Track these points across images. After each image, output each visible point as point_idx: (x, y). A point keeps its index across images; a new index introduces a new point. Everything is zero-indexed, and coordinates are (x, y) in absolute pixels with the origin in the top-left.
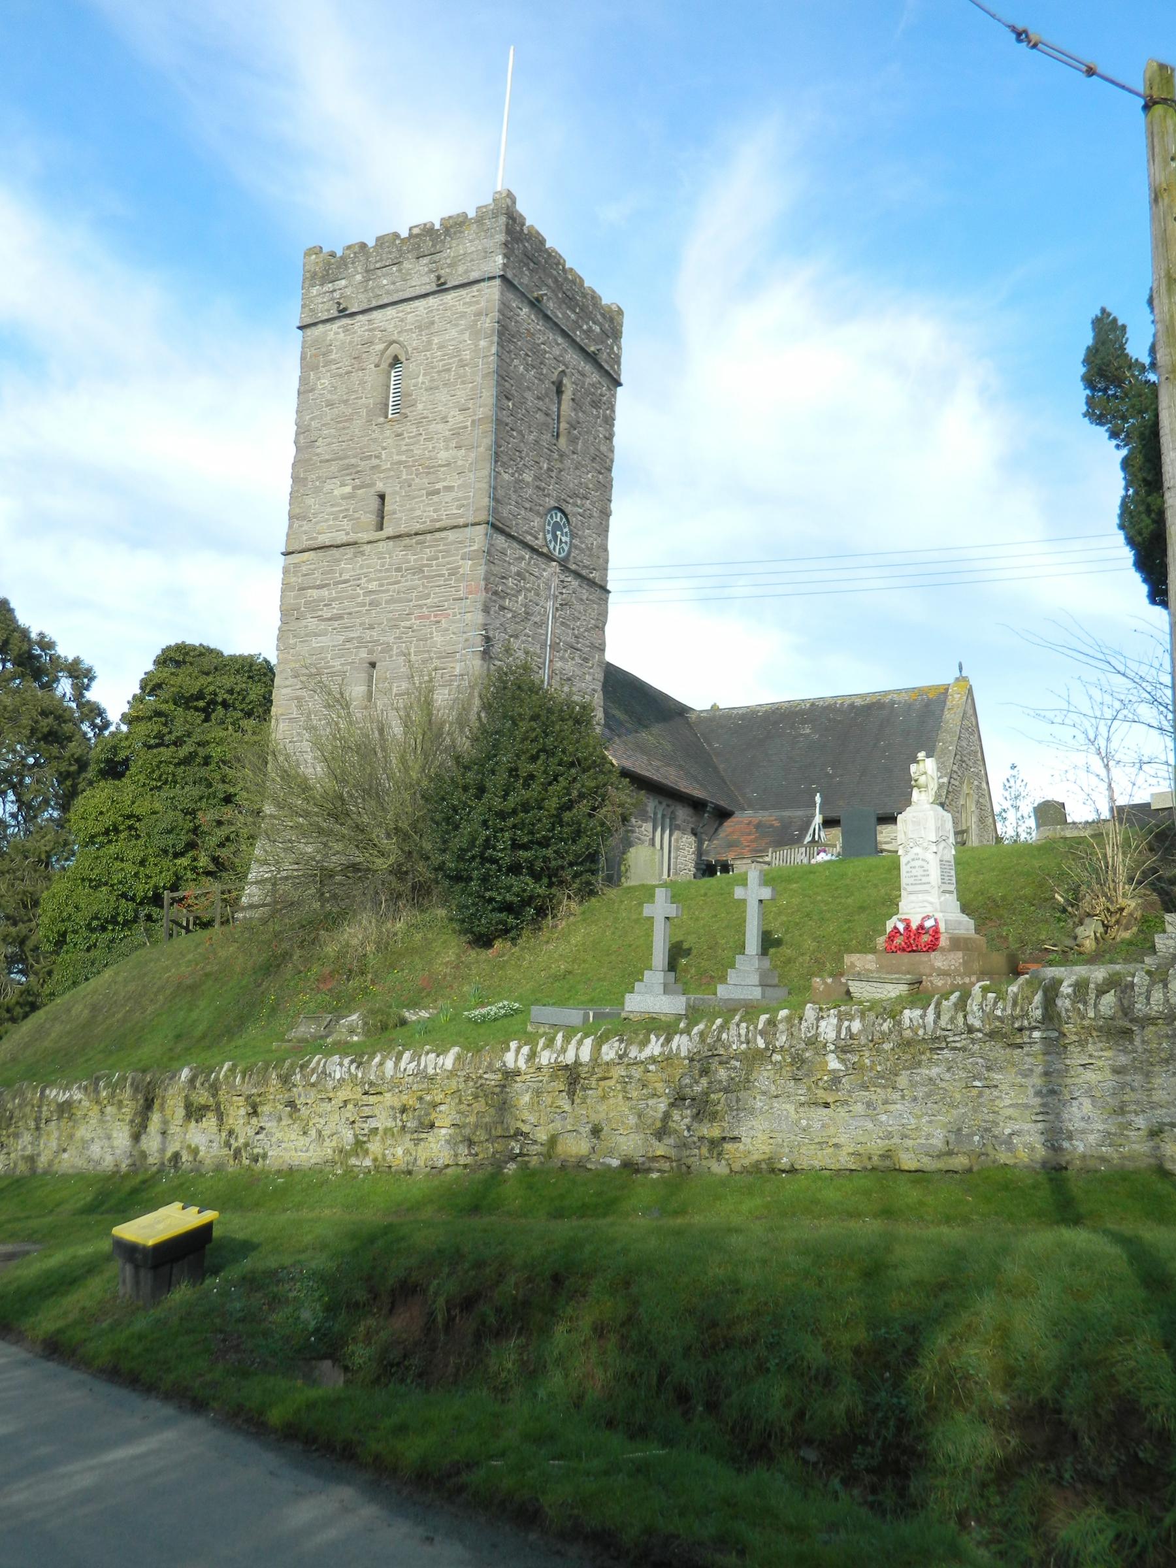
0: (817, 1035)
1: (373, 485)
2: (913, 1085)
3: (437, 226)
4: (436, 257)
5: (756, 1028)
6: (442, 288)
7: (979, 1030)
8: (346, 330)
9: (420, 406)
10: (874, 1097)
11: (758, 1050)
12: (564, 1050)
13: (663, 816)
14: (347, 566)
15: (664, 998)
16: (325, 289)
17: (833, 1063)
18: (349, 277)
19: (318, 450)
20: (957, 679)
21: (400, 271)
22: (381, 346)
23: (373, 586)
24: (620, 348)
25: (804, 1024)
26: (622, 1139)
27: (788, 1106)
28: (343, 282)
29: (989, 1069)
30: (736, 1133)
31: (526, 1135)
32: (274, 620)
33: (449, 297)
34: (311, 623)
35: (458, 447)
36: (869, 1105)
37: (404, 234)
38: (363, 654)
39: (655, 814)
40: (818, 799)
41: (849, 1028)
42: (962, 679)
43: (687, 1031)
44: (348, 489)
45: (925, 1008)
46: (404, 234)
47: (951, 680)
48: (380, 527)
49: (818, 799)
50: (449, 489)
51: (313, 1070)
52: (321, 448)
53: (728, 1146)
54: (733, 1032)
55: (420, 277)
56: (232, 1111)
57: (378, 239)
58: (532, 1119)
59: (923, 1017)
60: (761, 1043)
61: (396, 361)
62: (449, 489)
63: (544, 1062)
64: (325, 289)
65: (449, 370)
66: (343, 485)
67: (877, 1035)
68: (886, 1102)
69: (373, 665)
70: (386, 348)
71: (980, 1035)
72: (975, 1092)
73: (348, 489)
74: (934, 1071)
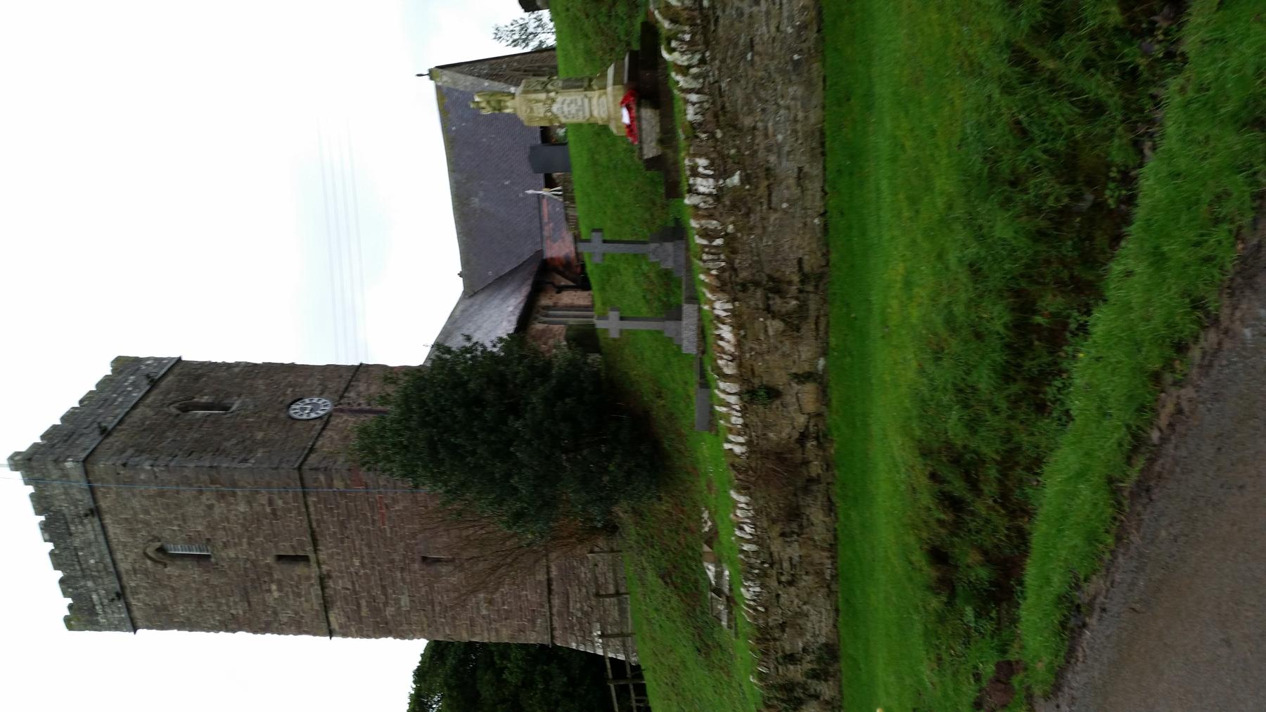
0: (710, 195)
1: (268, 565)
2: (751, 112)
3: (42, 518)
4: (69, 518)
5: (705, 246)
6: (95, 512)
7: (703, 54)
8: (135, 592)
9: (200, 528)
10: (762, 146)
11: (726, 244)
12: (728, 405)
13: (547, 316)
14: (338, 585)
15: (684, 322)
16: (100, 611)
17: (736, 179)
18: (89, 590)
19: (241, 612)
20: (431, 78)
21: (82, 549)
22: (149, 562)
23: (357, 563)
24: (148, 359)
25: (702, 205)
26: (803, 357)
27: (772, 219)
28: (95, 597)
29: (736, 45)
30: (795, 262)
31: (802, 434)
32: (388, 643)
33: (104, 504)
34: (390, 611)
35: (234, 494)
36: (769, 149)
37: (50, 546)
38: (416, 566)
39: (545, 322)
40: (530, 192)
41: (705, 168)
42: (432, 74)
43: (711, 302)
44: (274, 587)
45: (687, 102)
46: (50, 546)
47: (432, 84)
48: (305, 559)
49: (530, 192)
50: (271, 502)
51: (756, 610)
52: (239, 611)
53: (807, 268)
54: (710, 265)
55: (89, 529)
56: (790, 675)
57: (56, 568)
58: (787, 430)
59: (693, 104)
60: (719, 242)
61: (161, 550)
62: (271, 502)
63: (740, 421)
64: (100, 611)
65: (168, 505)
66: (269, 591)
67: (710, 143)
68: (766, 136)
69: (424, 559)
70: (150, 558)
71: (707, 54)
72: (757, 58)
73: (274, 587)
74: (739, 93)
